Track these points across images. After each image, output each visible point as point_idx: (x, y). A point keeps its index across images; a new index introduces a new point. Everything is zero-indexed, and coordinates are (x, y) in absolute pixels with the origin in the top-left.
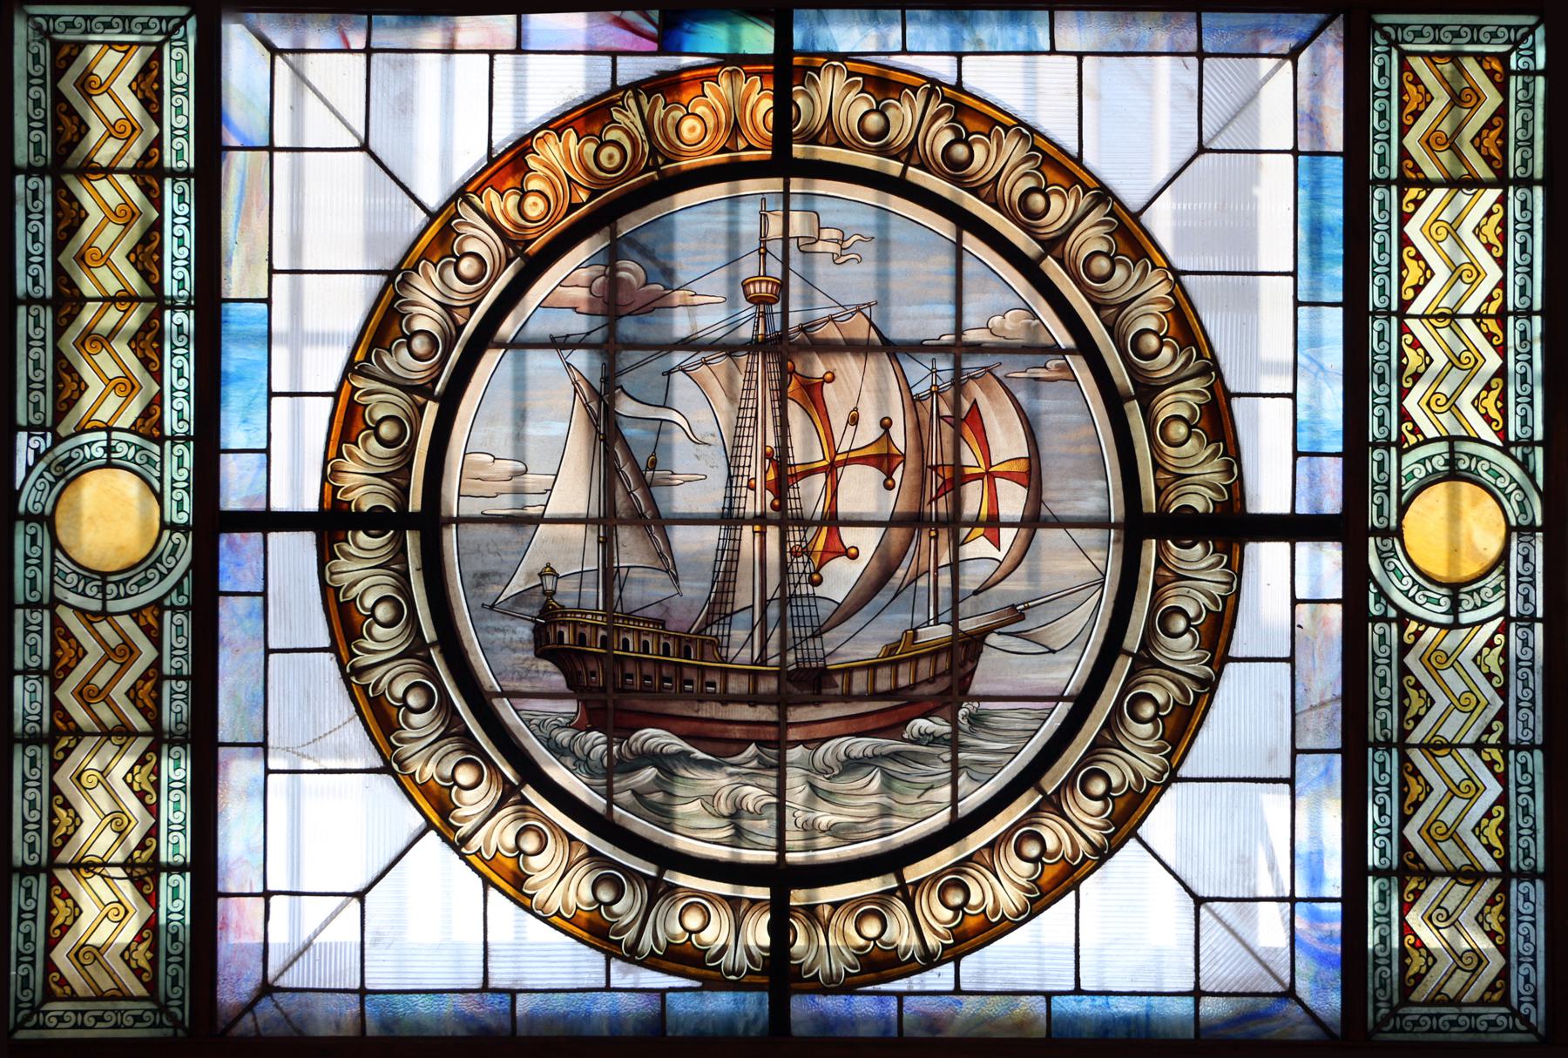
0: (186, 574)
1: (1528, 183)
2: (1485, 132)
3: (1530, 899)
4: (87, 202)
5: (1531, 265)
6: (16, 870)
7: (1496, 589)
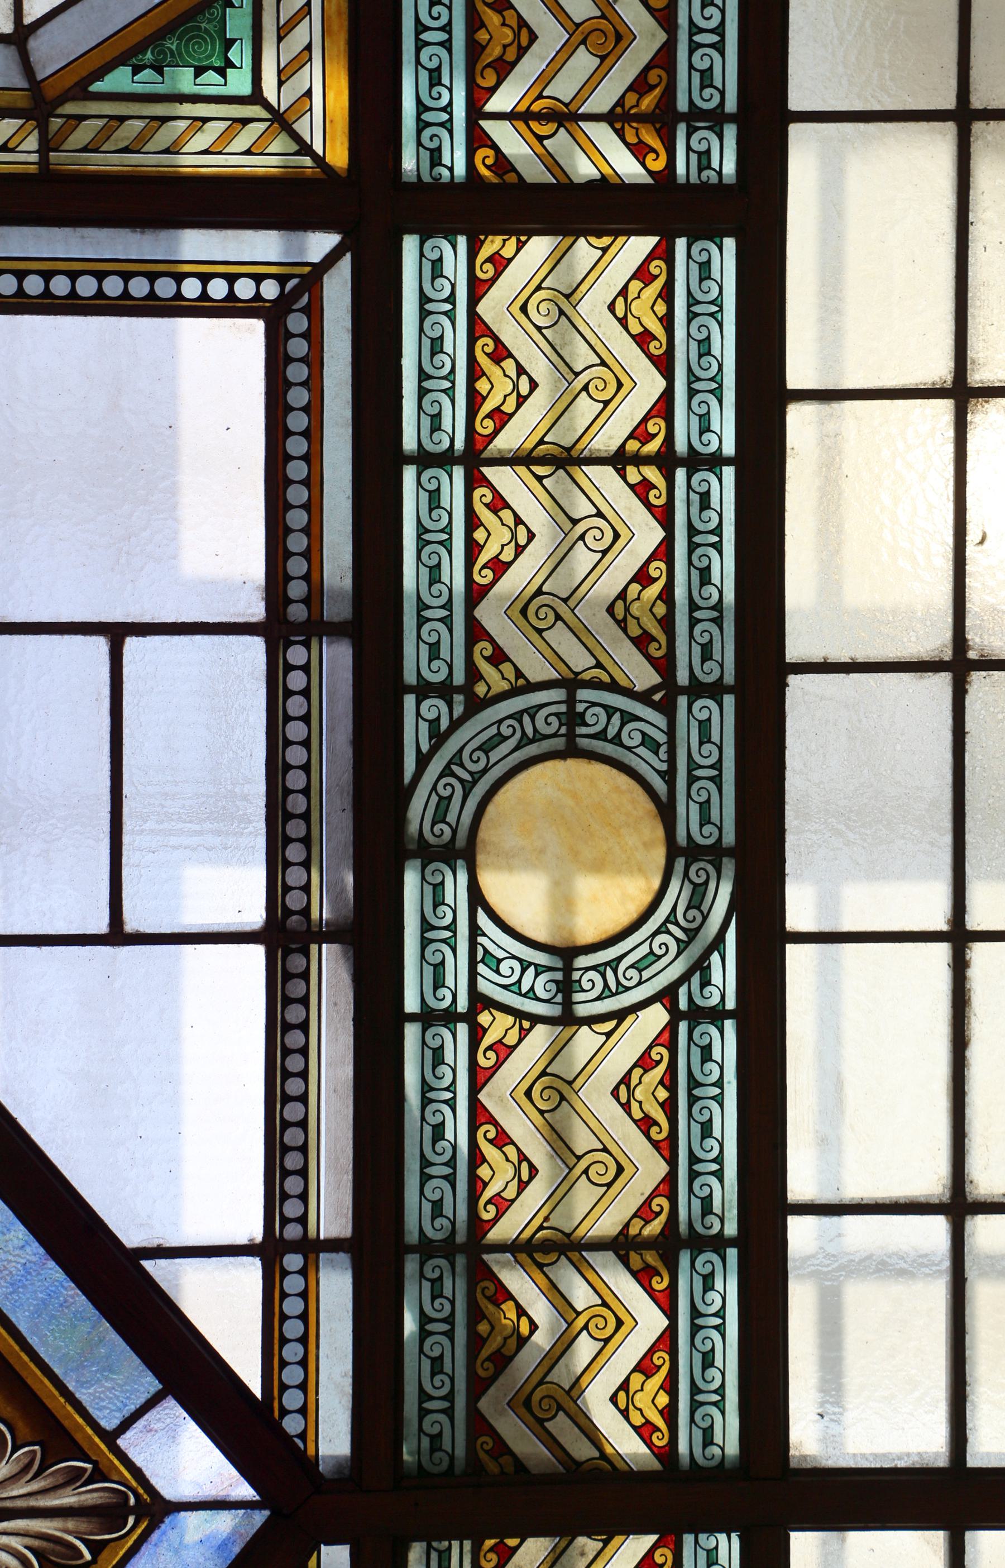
1: (428, 1018)
2: (510, 56)
5: (425, 943)
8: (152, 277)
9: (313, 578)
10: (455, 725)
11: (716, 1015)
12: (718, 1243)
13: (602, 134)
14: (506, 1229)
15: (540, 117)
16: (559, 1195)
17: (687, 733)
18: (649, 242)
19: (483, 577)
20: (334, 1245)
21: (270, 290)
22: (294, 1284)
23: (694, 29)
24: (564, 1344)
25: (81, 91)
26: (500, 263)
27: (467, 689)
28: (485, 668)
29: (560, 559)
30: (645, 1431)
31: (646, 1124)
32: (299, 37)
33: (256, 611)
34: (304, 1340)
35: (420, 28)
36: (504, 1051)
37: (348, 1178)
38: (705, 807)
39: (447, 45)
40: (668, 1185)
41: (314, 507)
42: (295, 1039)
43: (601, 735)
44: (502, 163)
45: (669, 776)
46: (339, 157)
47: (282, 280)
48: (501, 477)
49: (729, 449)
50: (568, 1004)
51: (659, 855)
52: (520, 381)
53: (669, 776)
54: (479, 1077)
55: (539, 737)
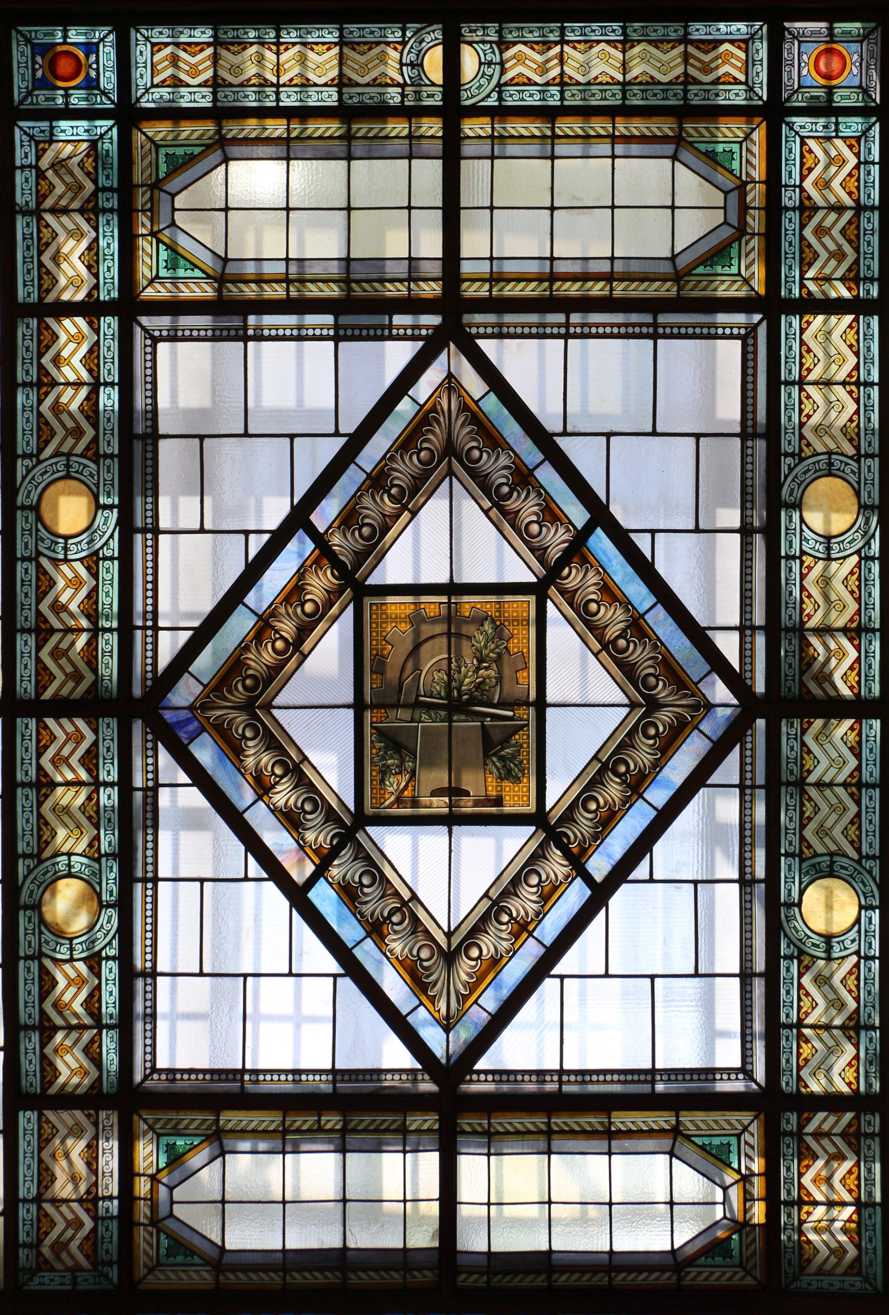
0: (114, 937)
3: (872, 799)
4: (59, 977)
6: (21, 1200)
7: (853, 941)
8: (709, 328)
9: (754, 419)
10: (796, 466)
11: (873, 559)
12: (873, 631)
13: (838, 284)
14: (812, 624)
15: (821, 279)
16: (826, 614)
17: (864, 470)
18: (852, 317)
19: (804, 420)
20: (760, 628)
21: (743, 331)
22: (748, 639)
23: (865, 253)
24: (827, 661)
25: (689, 273)
26: (809, 323)
27: (799, 455)
28: (805, 448)
29: (827, 368)
30: (851, 688)
31: (852, 592)
32: (751, 256)
33: (738, 430)
34: (751, 657)
35: (786, 253)
36: (810, 568)
37: (764, 607)
38: (869, 493)
39: (794, 258)
40: (858, 612)
41: (755, 398)
42: (749, 571)
43: (839, 470)
44: (810, 293)
45: (859, 483)
46: (762, 291)
47: (746, 328)
48: (810, 389)
49: (876, 380)
50: (829, 554)
51: (856, 507)
52: (804, 897)
53: (859, 483)
54: (803, 577)
55: (820, 470)
